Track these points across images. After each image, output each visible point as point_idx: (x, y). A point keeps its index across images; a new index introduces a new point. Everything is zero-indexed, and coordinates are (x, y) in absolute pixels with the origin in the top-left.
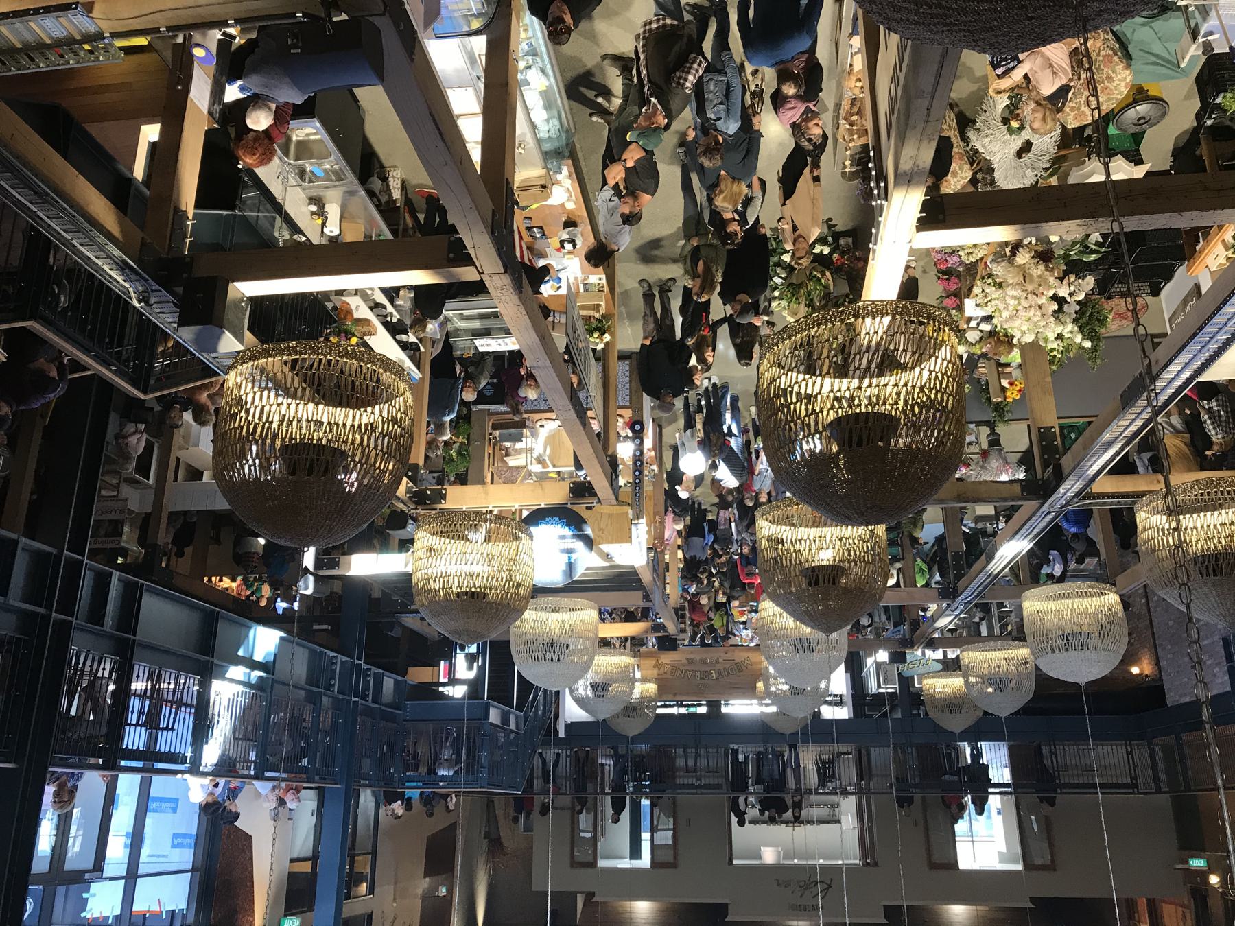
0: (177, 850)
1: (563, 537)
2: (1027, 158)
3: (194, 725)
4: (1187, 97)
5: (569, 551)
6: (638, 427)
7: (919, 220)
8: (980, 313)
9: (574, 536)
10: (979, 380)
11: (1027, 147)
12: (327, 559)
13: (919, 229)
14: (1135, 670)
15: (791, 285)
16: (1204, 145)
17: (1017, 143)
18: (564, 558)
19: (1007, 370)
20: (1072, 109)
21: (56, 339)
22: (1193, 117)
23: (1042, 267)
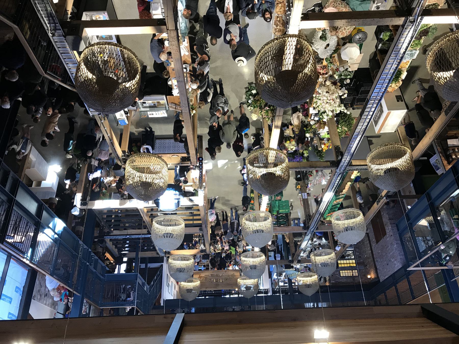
0: (67, 121)
1: (176, 194)
2: (328, 48)
3: (31, 243)
4: (373, 40)
5: (179, 199)
6: (201, 159)
7: (302, 18)
8: (316, 112)
9: (180, 194)
10: (314, 145)
11: (328, 45)
12: (84, 202)
13: (301, 20)
14: (369, 277)
15: (255, 100)
16: (378, 55)
17: (325, 44)
18: (177, 201)
19: (323, 142)
20: (340, 32)
21: (8, 22)
22: (374, 47)
23: (334, 87)
